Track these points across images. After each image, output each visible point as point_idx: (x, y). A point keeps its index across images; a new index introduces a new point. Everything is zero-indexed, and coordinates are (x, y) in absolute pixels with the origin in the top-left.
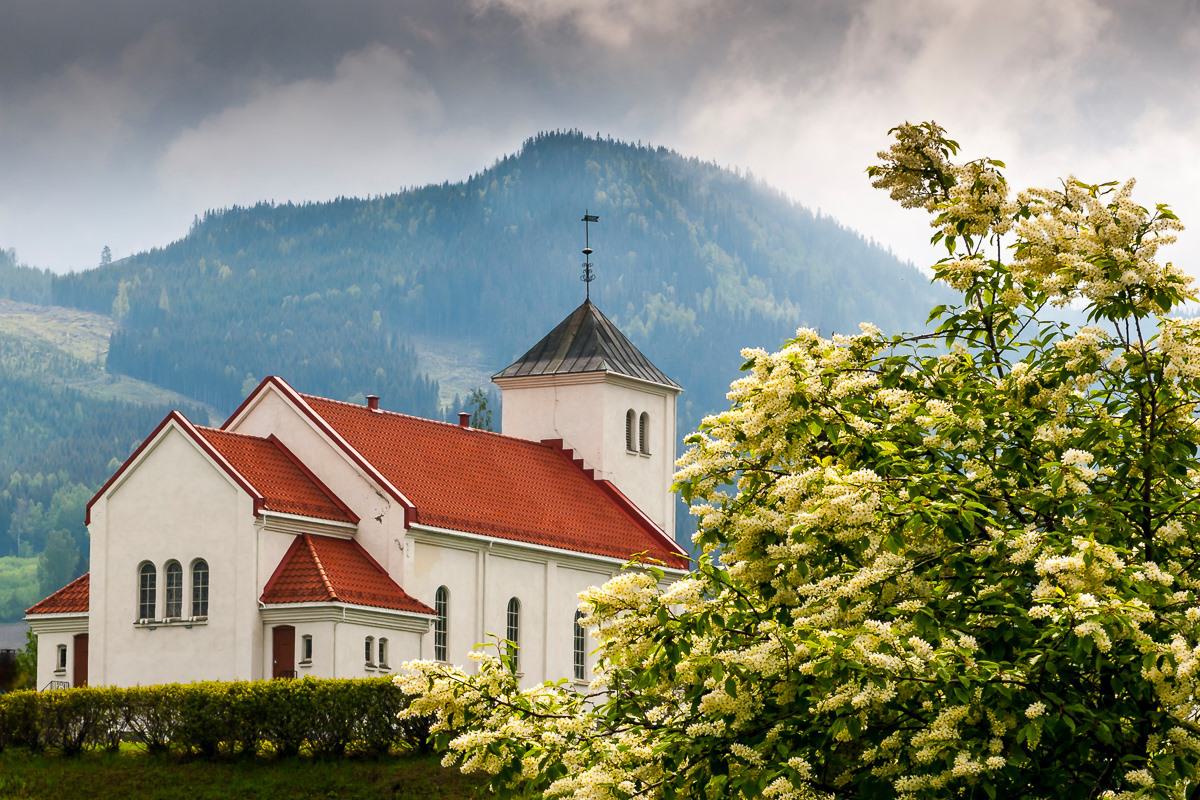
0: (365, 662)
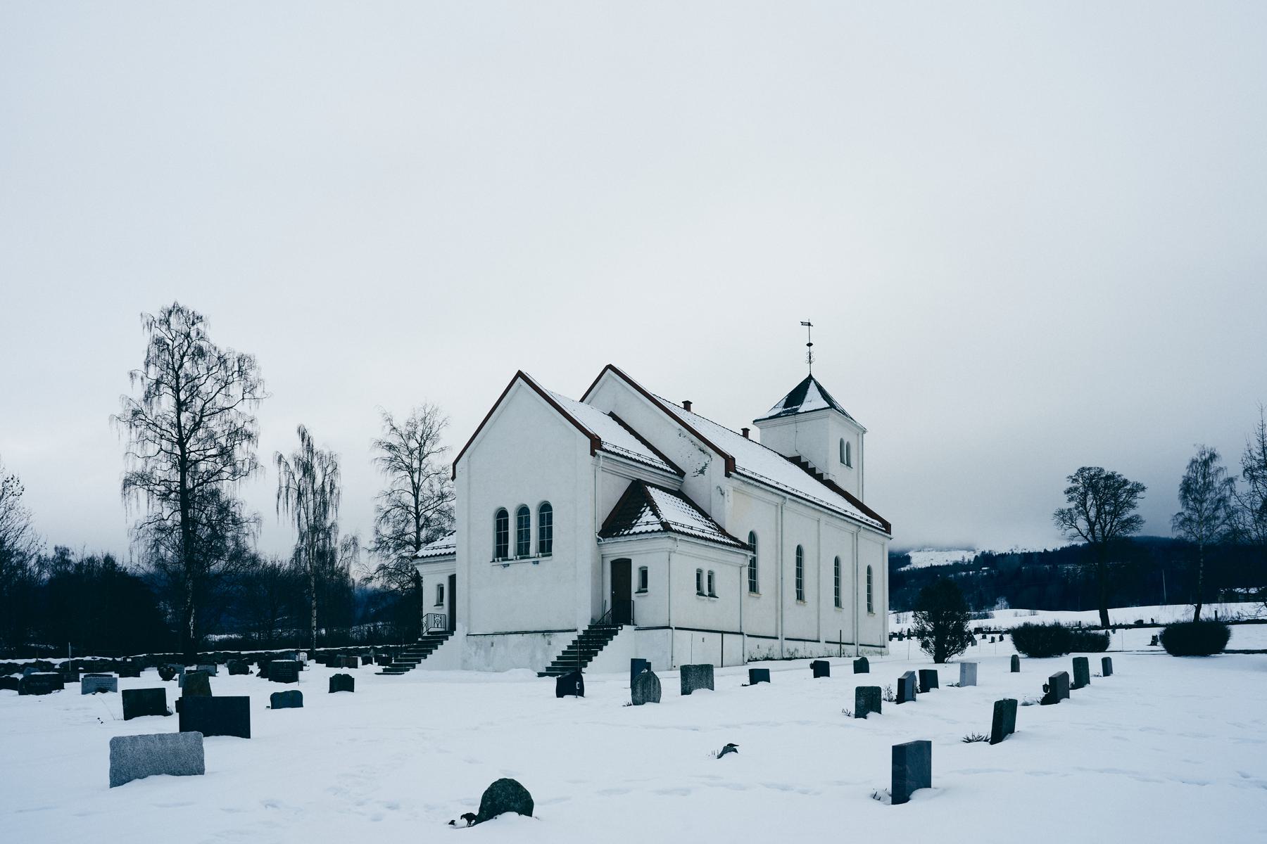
0: (696, 591)
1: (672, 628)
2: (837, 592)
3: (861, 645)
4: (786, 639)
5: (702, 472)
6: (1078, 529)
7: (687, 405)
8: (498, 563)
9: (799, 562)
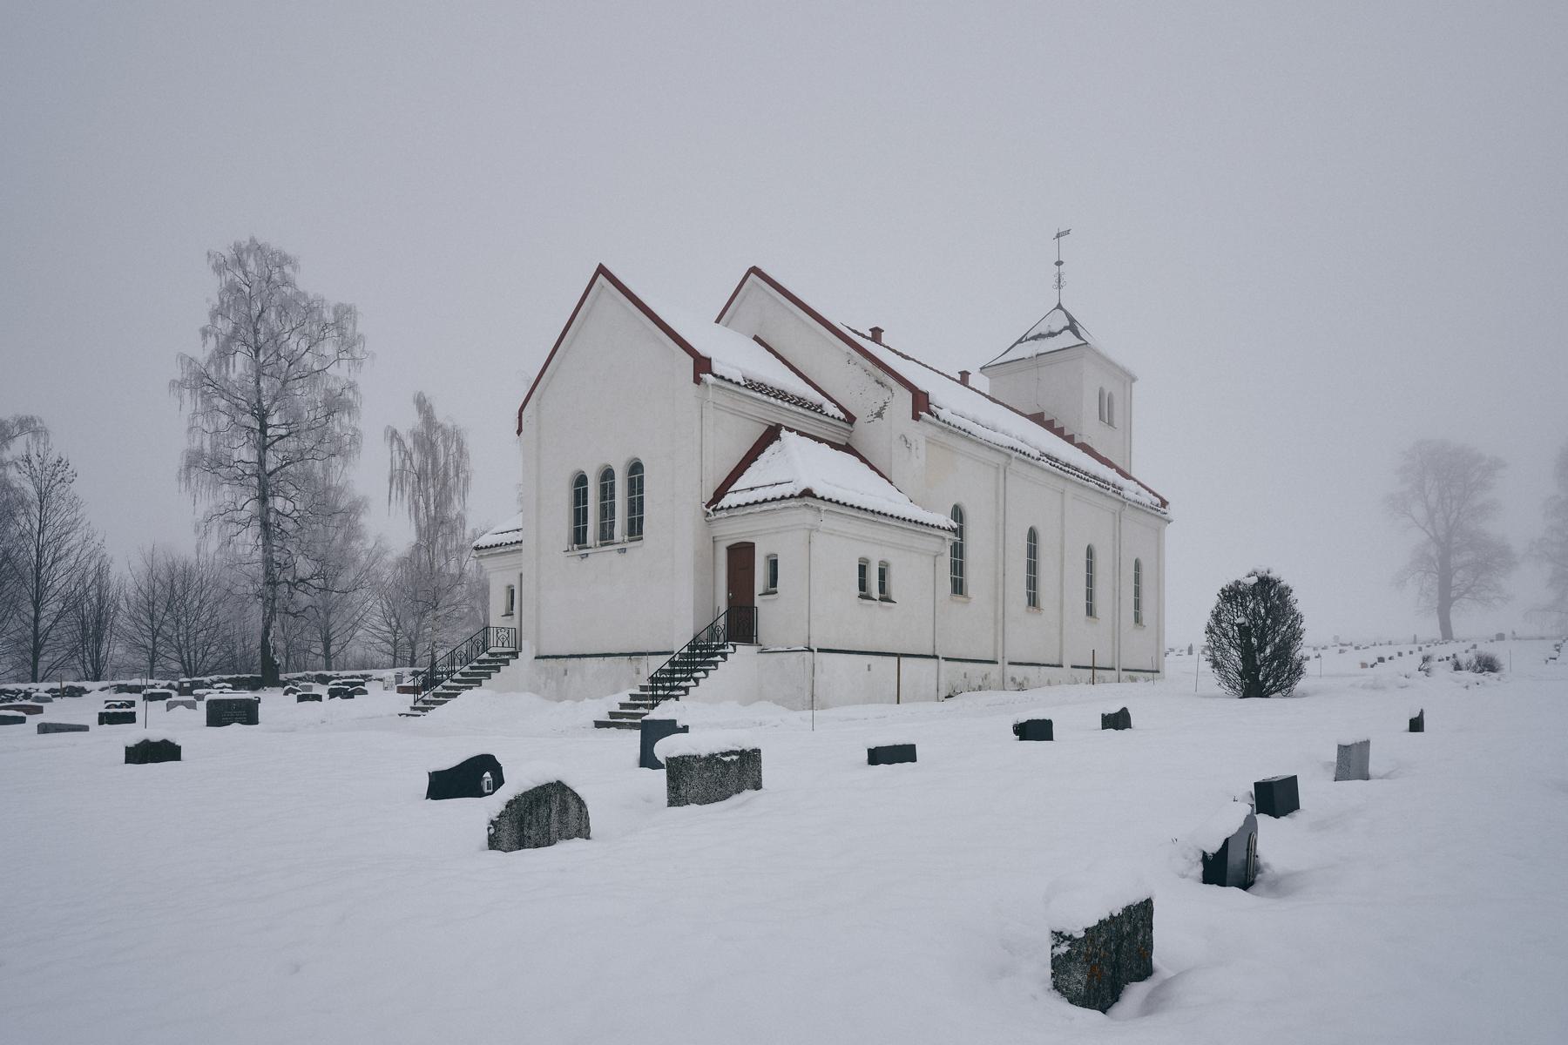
0: (857, 591)
1: (813, 651)
2: (1090, 595)
3: (1124, 670)
4: (1010, 663)
5: (879, 415)
6: (1414, 519)
7: (876, 334)
8: (573, 553)
9: (1032, 552)
